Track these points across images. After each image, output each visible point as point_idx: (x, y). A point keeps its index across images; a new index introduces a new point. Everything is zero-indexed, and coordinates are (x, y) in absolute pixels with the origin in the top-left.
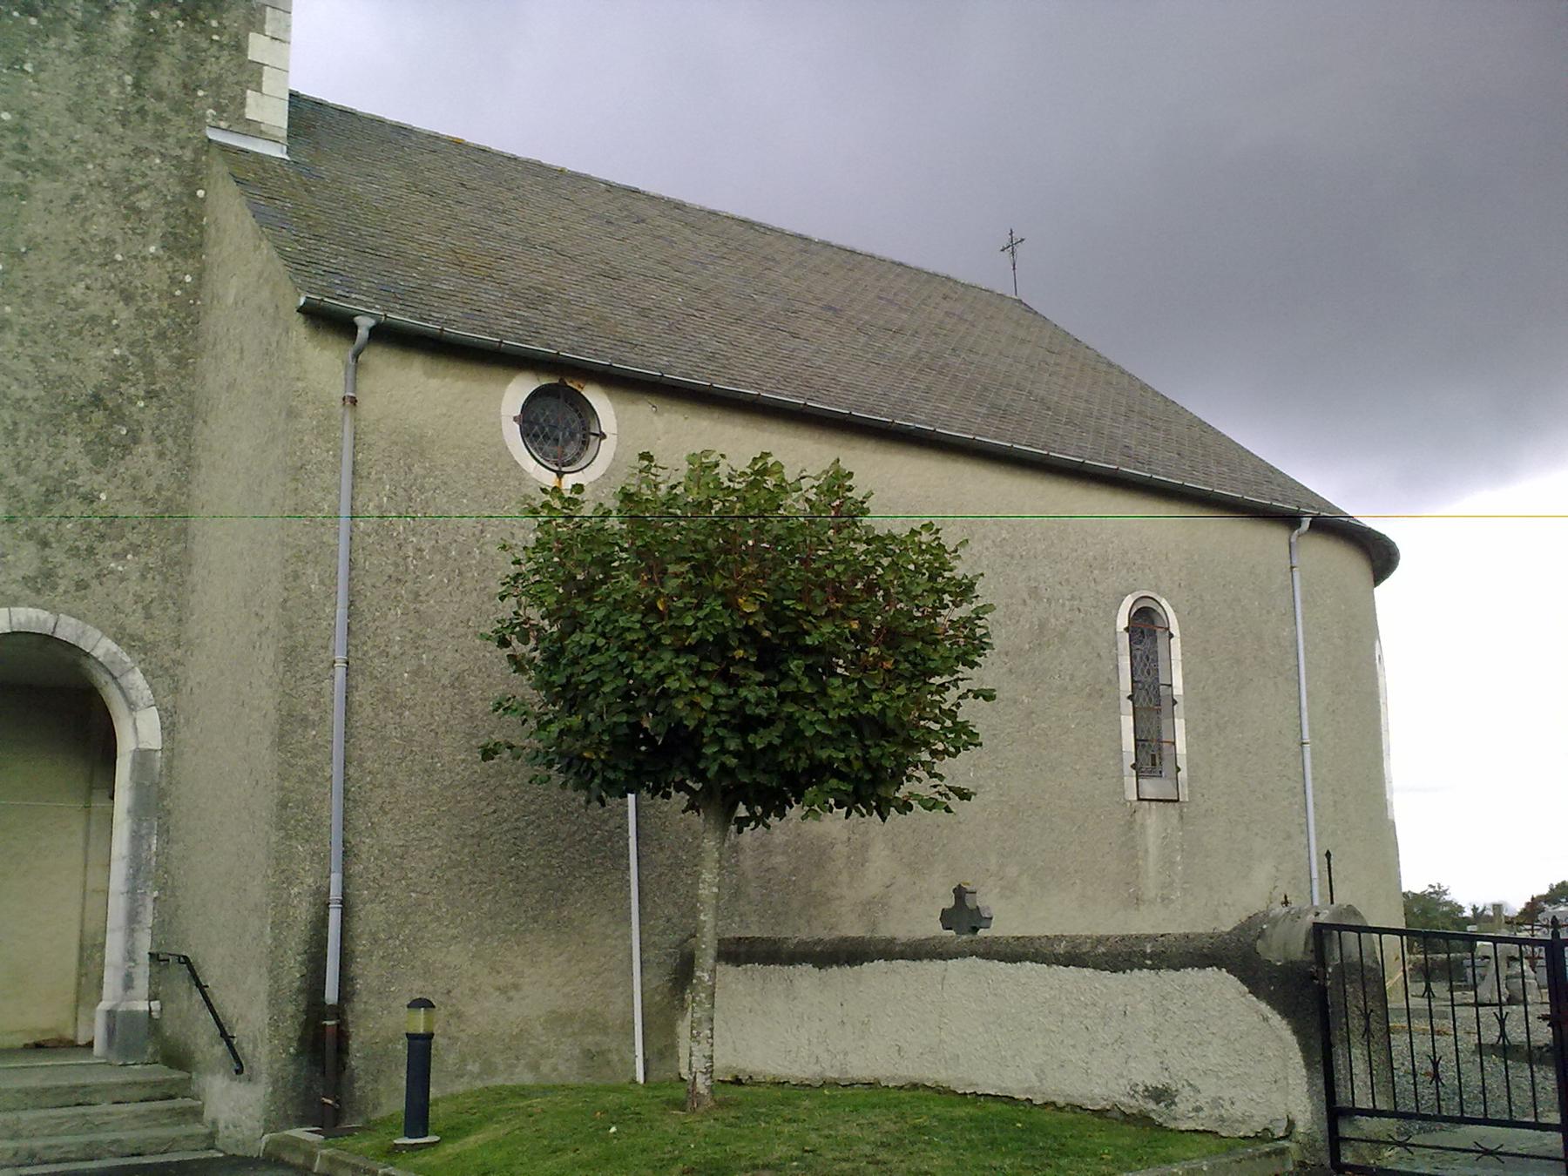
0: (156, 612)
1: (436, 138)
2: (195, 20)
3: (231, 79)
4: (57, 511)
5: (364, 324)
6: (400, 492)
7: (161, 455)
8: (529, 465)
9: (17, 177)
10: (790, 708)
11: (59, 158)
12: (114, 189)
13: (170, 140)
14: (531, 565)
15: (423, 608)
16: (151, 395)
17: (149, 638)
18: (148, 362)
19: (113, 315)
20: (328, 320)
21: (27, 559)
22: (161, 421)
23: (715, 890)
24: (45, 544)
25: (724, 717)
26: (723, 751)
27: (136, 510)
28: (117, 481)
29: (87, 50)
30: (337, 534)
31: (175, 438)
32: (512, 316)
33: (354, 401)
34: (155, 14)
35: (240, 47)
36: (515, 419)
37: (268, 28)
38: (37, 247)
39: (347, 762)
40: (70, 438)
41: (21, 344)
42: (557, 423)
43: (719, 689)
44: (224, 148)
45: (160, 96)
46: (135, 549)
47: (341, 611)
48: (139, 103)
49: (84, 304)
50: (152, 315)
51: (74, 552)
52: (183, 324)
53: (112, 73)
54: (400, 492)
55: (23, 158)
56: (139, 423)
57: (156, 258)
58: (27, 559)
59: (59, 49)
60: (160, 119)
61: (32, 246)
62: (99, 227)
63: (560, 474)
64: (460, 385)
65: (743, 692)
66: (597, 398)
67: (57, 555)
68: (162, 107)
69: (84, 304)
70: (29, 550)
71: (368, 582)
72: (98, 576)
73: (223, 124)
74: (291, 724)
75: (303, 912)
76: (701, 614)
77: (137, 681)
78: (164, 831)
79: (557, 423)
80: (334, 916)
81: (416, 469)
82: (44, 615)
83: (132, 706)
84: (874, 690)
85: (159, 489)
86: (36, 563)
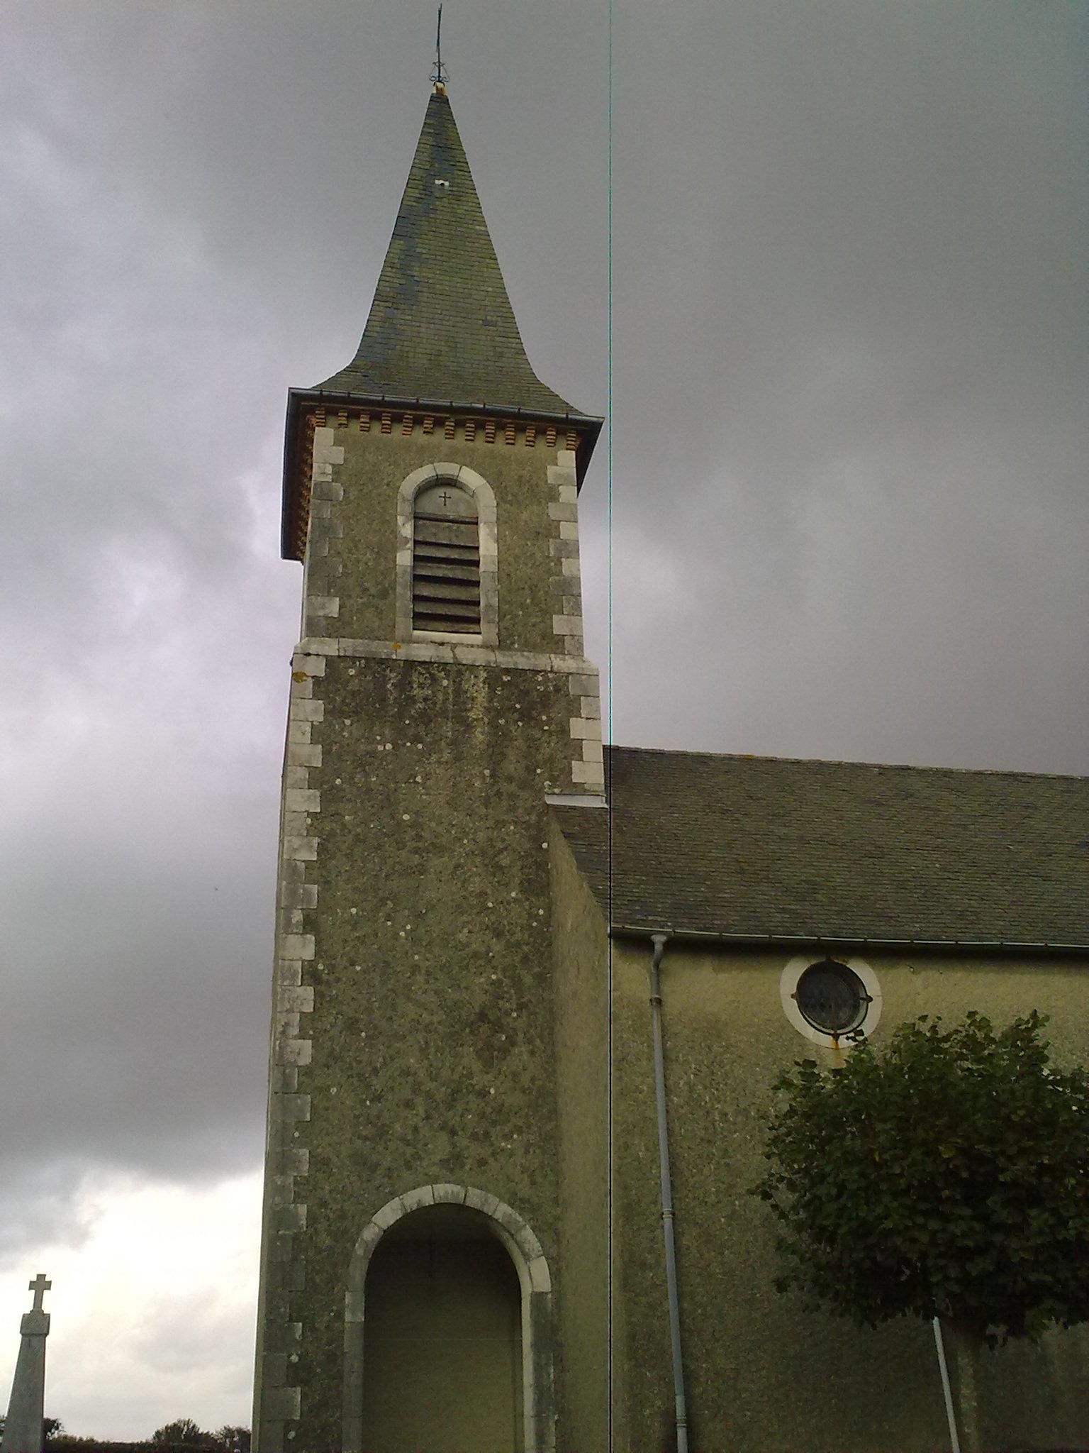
0: (539, 1180)
1: (730, 758)
2: (531, 718)
3: (560, 756)
4: (460, 1107)
5: (659, 940)
6: (704, 1069)
7: (532, 1053)
8: (809, 1032)
9: (416, 859)
10: (997, 1238)
11: (444, 839)
12: (483, 854)
13: (520, 811)
14: (783, 1130)
15: (731, 1162)
16: (521, 1007)
17: (536, 1200)
18: (517, 982)
19: (489, 950)
20: (632, 942)
21: (441, 1146)
22: (530, 1025)
23: (975, 1404)
24: (453, 1133)
25: (942, 1249)
26: (947, 1278)
27: (516, 1099)
28: (502, 1077)
29: (458, 758)
30: (656, 1109)
31: (541, 1037)
32: (784, 911)
33: (659, 1001)
34: (502, 722)
35: (564, 731)
36: (793, 996)
37: (584, 713)
38: (433, 908)
39: (680, 1297)
40: (466, 1048)
41: (427, 982)
42: (830, 997)
43: (934, 1225)
44: (556, 807)
45: (510, 779)
46: (519, 1130)
47: (664, 1171)
48: (496, 788)
49: (468, 945)
50: (518, 944)
51: (474, 1137)
52: (539, 948)
53: (476, 771)
54: (704, 1069)
55: (420, 844)
56: (514, 1029)
57: (516, 900)
58: (441, 1146)
59: (439, 762)
60: (512, 796)
61: (431, 908)
62: (475, 885)
63: (836, 1037)
64: (745, 975)
65: (951, 1227)
66: (862, 970)
67: (463, 1141)
68: (513, 787)
69: (468, 945)
70: (443, 1137)
71: (685, 1144)
72: (493, 1154)
73: (557, 791)
74: (634, 1267)
75: (656, 1429)
76: (905, 1163)
77: (528, 1235)
78: (559, 1361)
79: (830, 997)
80: (681, 1433)
81: (715, 1048)
82: (457, 1188)
83: (527, 1257)
84: (1070, 1218)
85: (533, 1080)
86: (449, 1149)
